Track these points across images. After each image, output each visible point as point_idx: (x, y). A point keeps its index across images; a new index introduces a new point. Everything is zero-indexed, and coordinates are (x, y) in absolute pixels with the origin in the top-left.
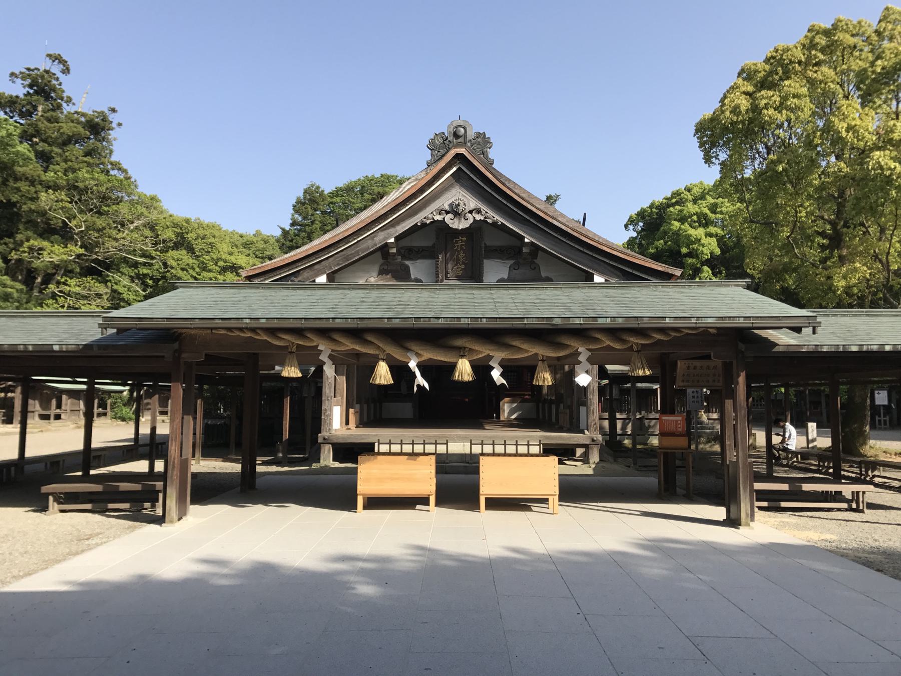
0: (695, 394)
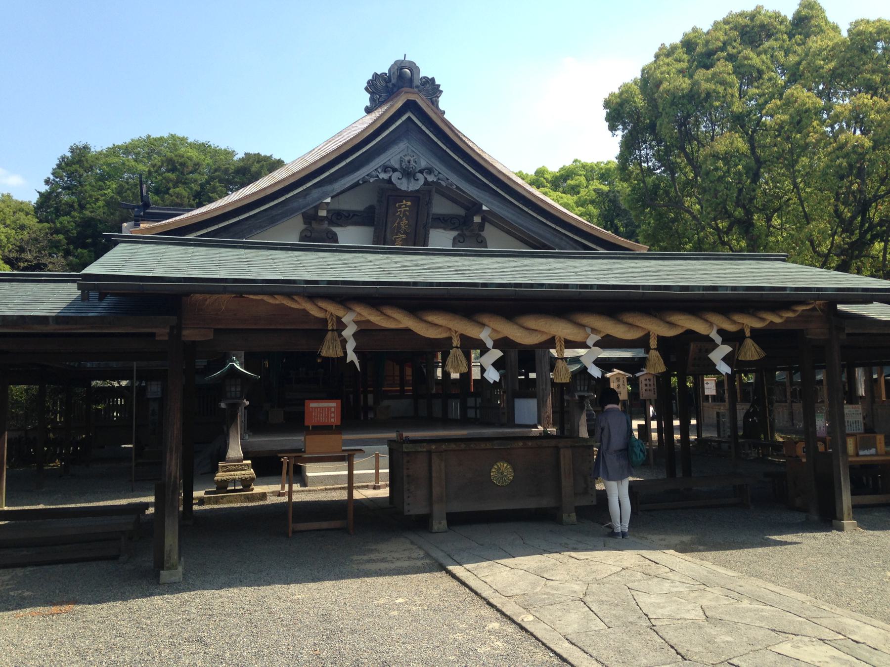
0: (648, 382)
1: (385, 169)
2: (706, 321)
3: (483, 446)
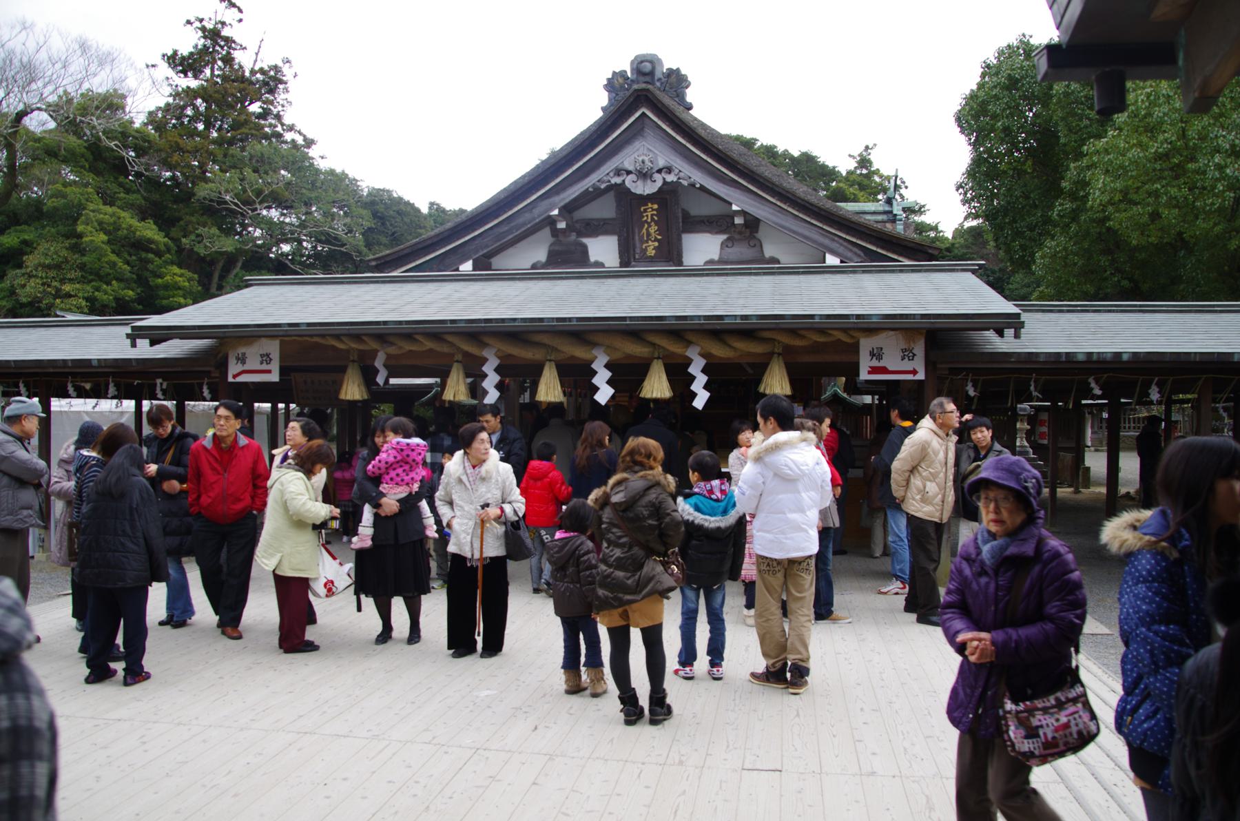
1: (618, 172)
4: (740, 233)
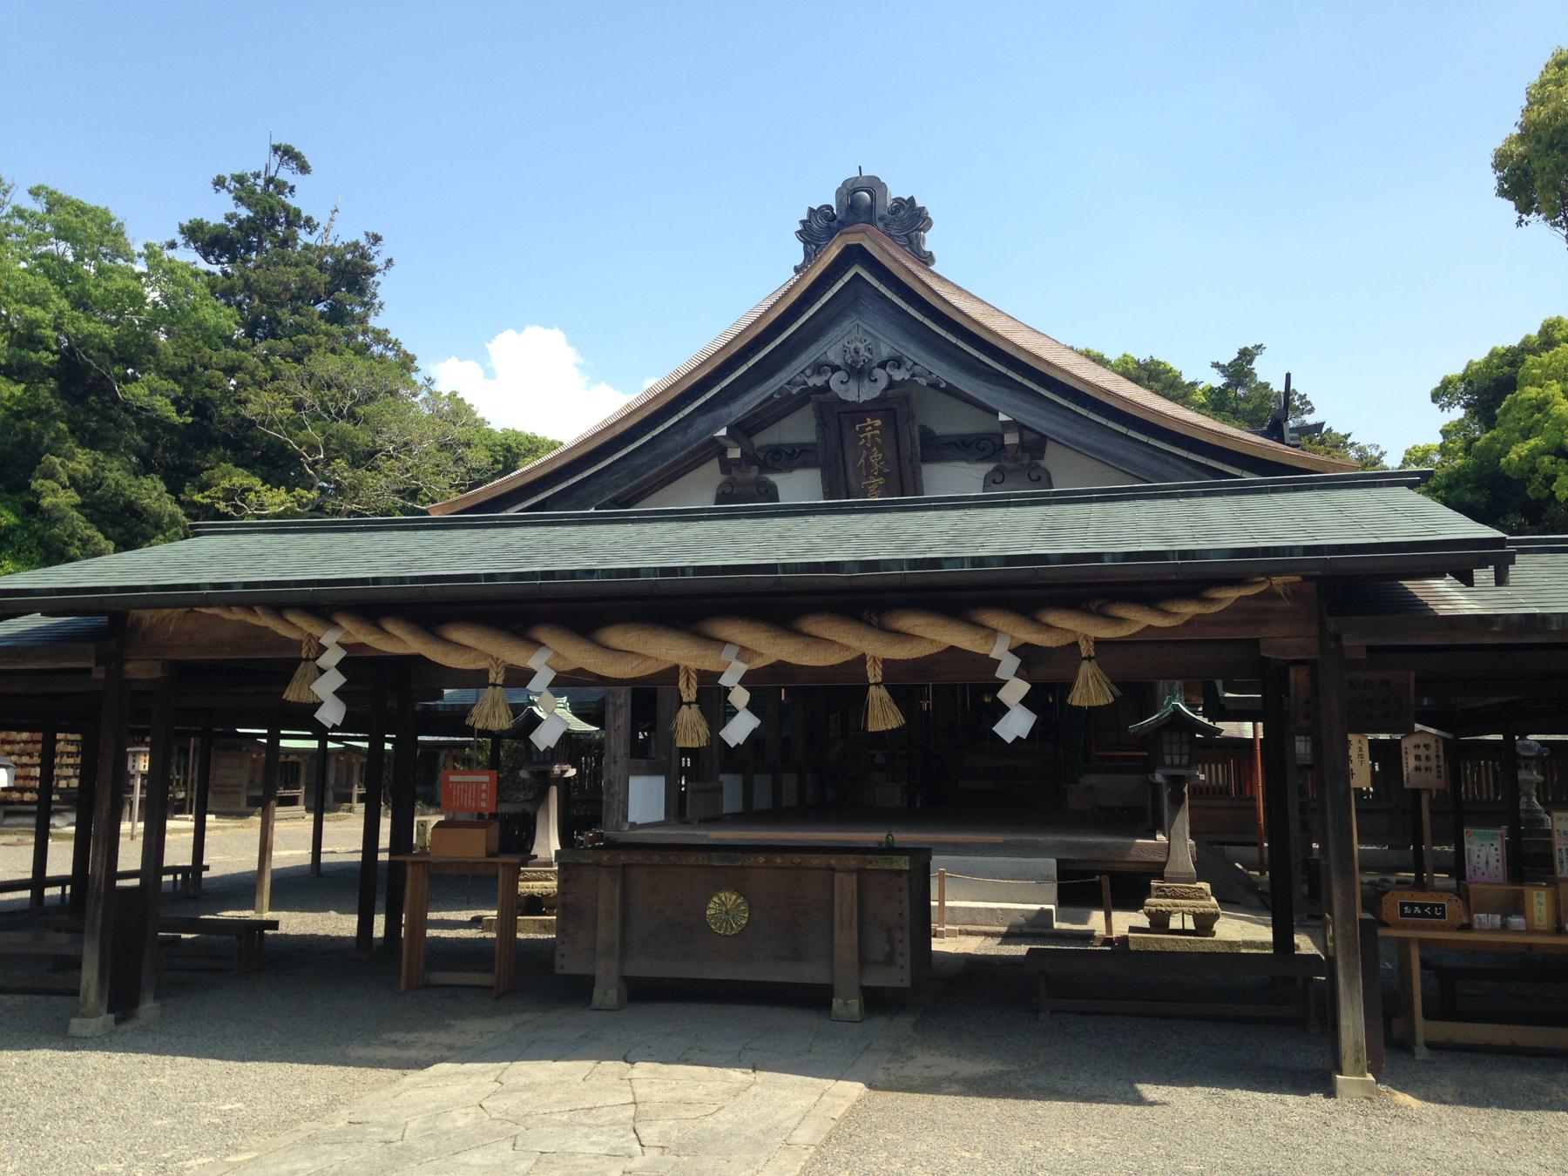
0: (1422, 752)
1: (818, 368)
2: (982, 626)
3: (692, 859)
4: (1015, 459)
